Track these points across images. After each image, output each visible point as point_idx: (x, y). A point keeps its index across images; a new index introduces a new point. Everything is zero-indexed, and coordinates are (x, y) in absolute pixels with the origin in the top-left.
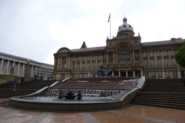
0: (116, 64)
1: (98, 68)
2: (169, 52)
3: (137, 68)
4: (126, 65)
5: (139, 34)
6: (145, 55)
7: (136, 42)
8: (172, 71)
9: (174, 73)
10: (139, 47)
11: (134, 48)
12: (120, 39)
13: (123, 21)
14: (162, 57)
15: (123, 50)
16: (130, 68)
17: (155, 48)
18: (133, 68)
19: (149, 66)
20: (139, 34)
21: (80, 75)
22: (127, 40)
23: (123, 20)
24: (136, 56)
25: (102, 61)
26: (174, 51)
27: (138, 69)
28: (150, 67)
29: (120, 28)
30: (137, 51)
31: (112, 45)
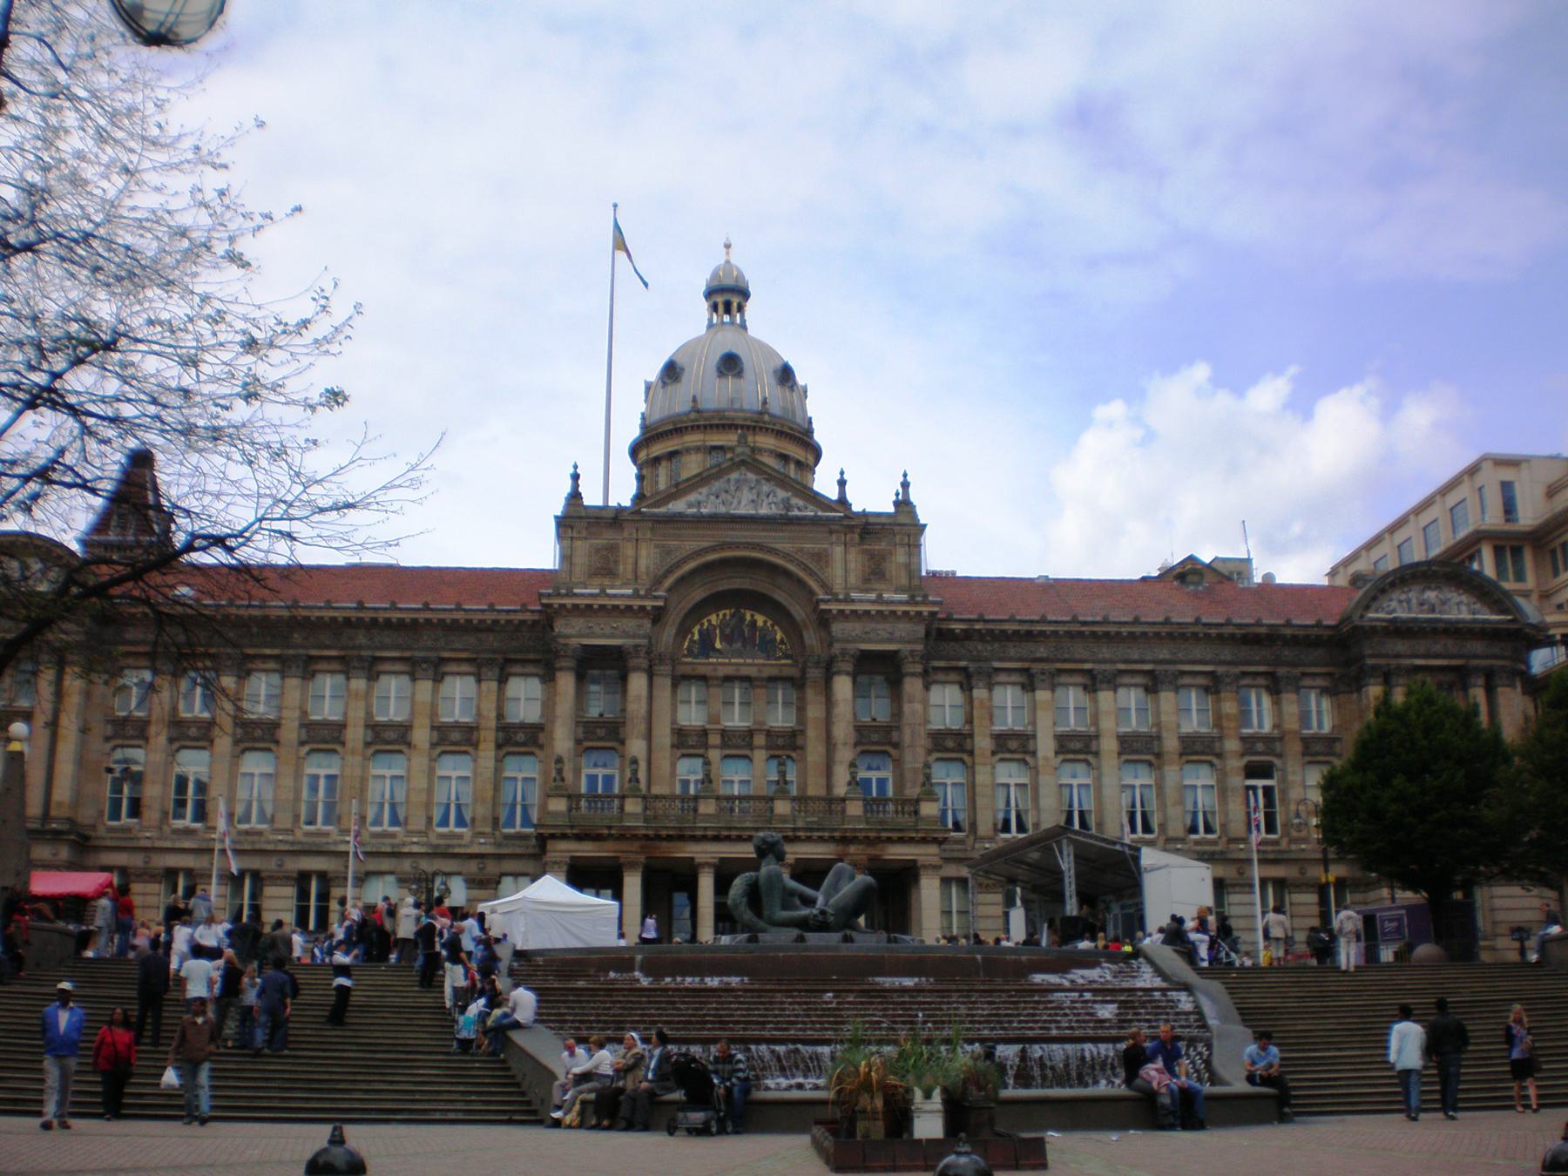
0: (811, 792)
1: (437, 815)
2: (1167, 698)
3: (889, 840)
4: (782, 807)
5: (576, 477)
6: (943, 705)
7: (875, 572)
8: (285, 879)
9: (303, 895)
10: (903, 628)
11: (854, 628)
12: (714, 520)
13: (704, 306)
14: (1109, 745)
15: (724, 638)
16: (821, 839)
17: (1042, 651)
18: (845, 840)
19: (984, 828)
20: (576, 477)
21: (269, 891)
22: (782, 543)
23: (710, 294)
24: (593, 712)
25: (488, 738)
26: (1207, 690)
27: (897, 852)
28: (991, 839)
29: (672, 371)
30: (881, 669)
31: (625, 568)
